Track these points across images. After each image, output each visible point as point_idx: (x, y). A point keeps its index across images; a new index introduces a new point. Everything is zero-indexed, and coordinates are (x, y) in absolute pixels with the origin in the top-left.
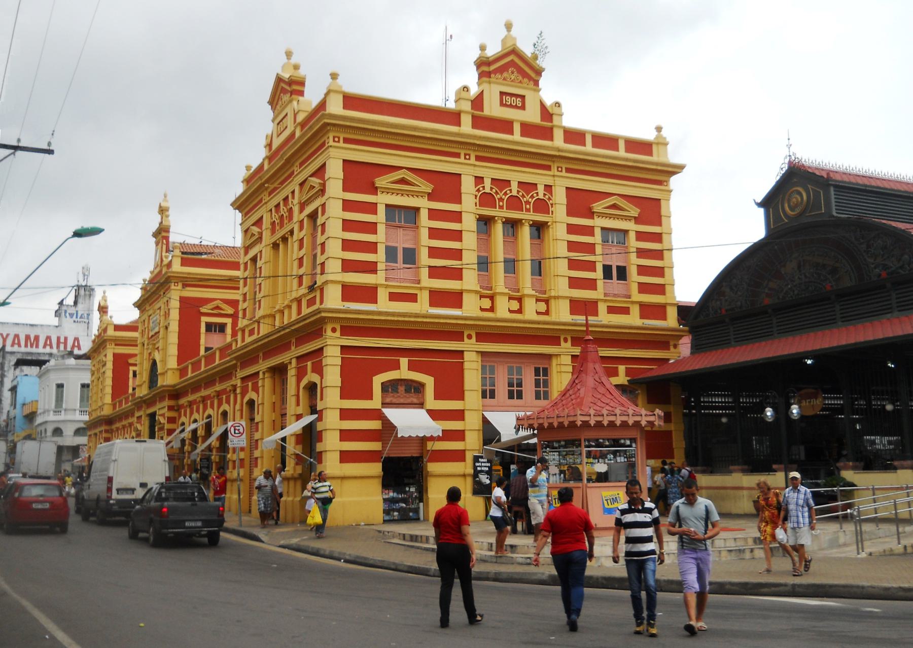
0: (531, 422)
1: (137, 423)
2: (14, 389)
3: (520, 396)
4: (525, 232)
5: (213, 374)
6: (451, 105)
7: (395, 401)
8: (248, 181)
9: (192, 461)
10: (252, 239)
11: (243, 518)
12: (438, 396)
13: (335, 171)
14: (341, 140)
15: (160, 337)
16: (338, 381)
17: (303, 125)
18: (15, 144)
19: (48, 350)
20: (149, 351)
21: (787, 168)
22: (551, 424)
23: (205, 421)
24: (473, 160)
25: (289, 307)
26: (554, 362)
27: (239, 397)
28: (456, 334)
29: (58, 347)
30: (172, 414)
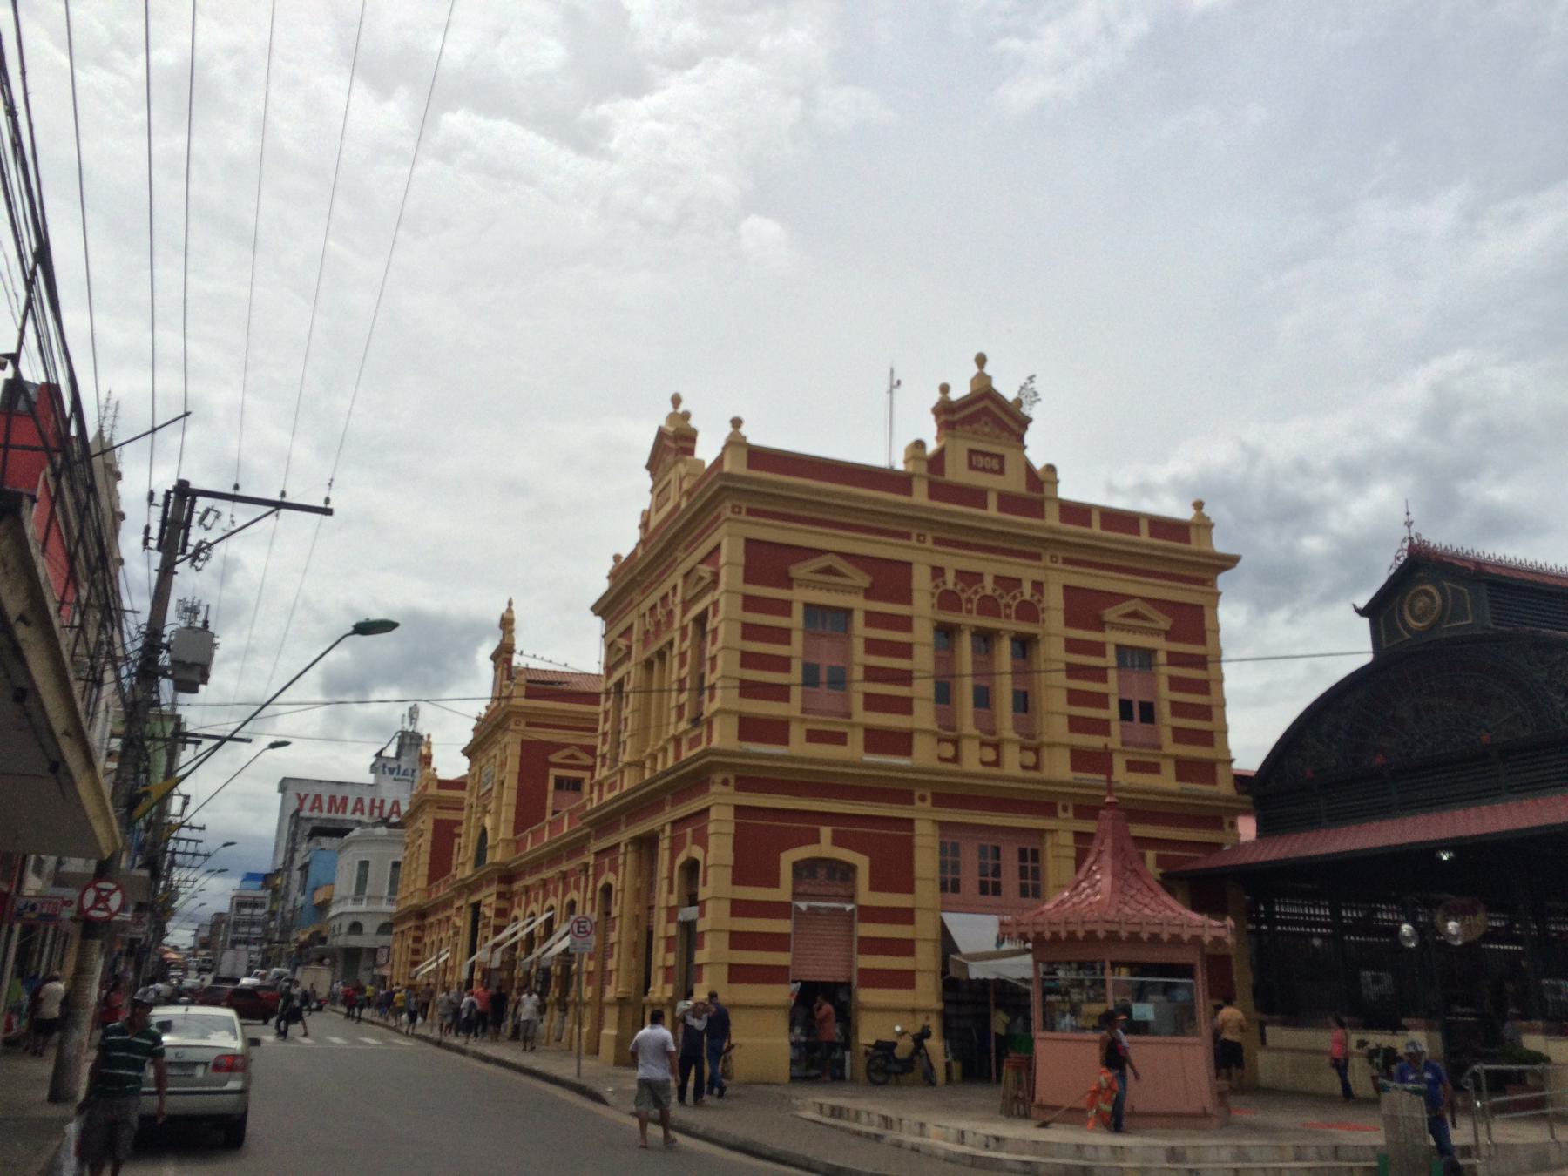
0: (1022, 929)
1: (456, 916)
2: (305, 868)
3: (997, 890)
4: (1005, 649)
5: (558, 849)
6: (900, 466)
7: (811, 890)
8: (612, 576)
9: (525, 973)
10: (615, 654)
11: (583, 1063)
12: (875, 886)
13: (732, 552)
14: (744, 511)
15: (494, 795)
16: (728, 857)
17: (689, 493)
18: (276, 497)
19: (357, 816)
20: (479, 815)
21: (1406, 556)
22: (1055, 935)
23: (546, 915)
24: (929, 544)
25: (664, 750)
26: (1049, 840)
27: (591, 880)
28: (903, 795)
29: (371, 813)
30: (503, 904)
